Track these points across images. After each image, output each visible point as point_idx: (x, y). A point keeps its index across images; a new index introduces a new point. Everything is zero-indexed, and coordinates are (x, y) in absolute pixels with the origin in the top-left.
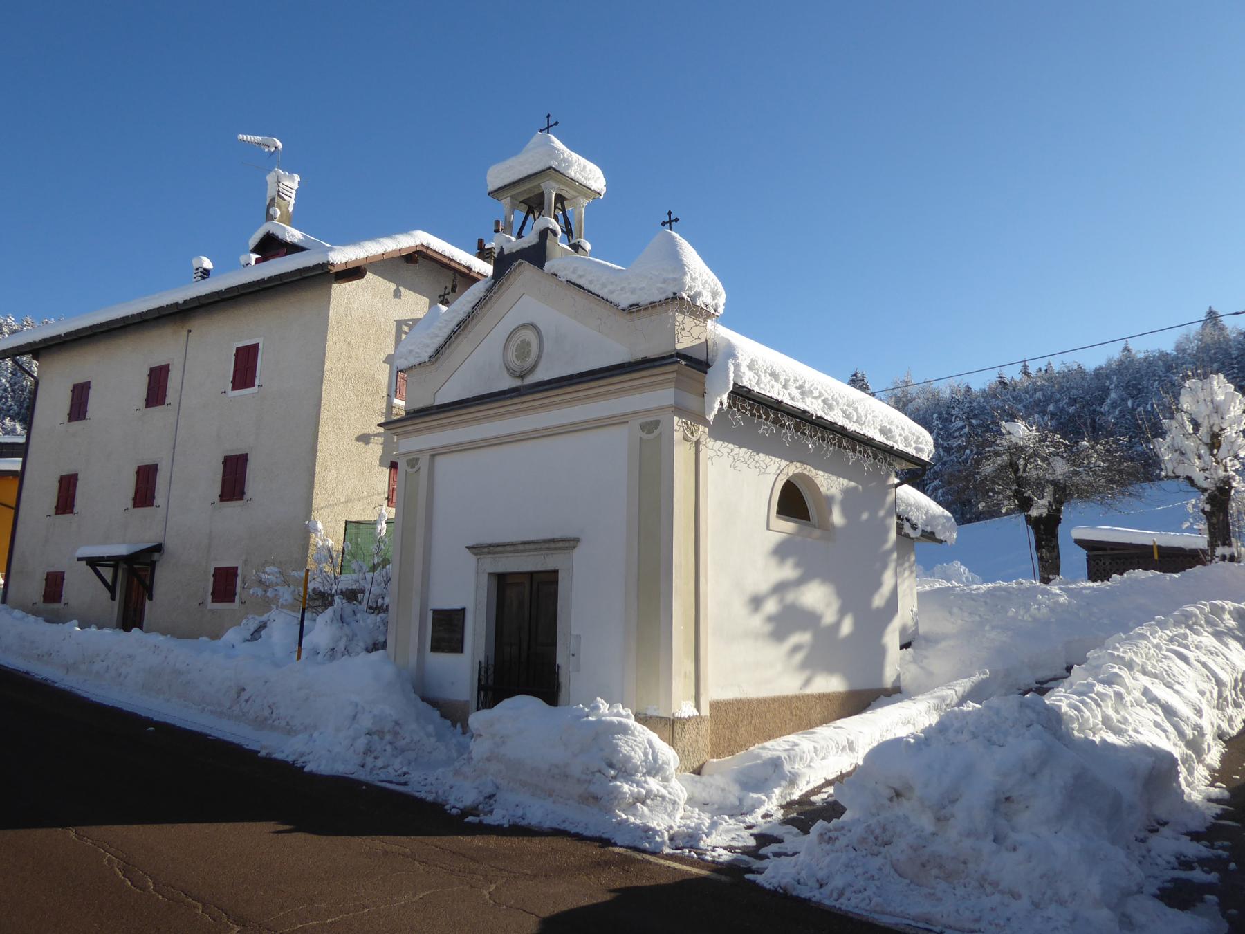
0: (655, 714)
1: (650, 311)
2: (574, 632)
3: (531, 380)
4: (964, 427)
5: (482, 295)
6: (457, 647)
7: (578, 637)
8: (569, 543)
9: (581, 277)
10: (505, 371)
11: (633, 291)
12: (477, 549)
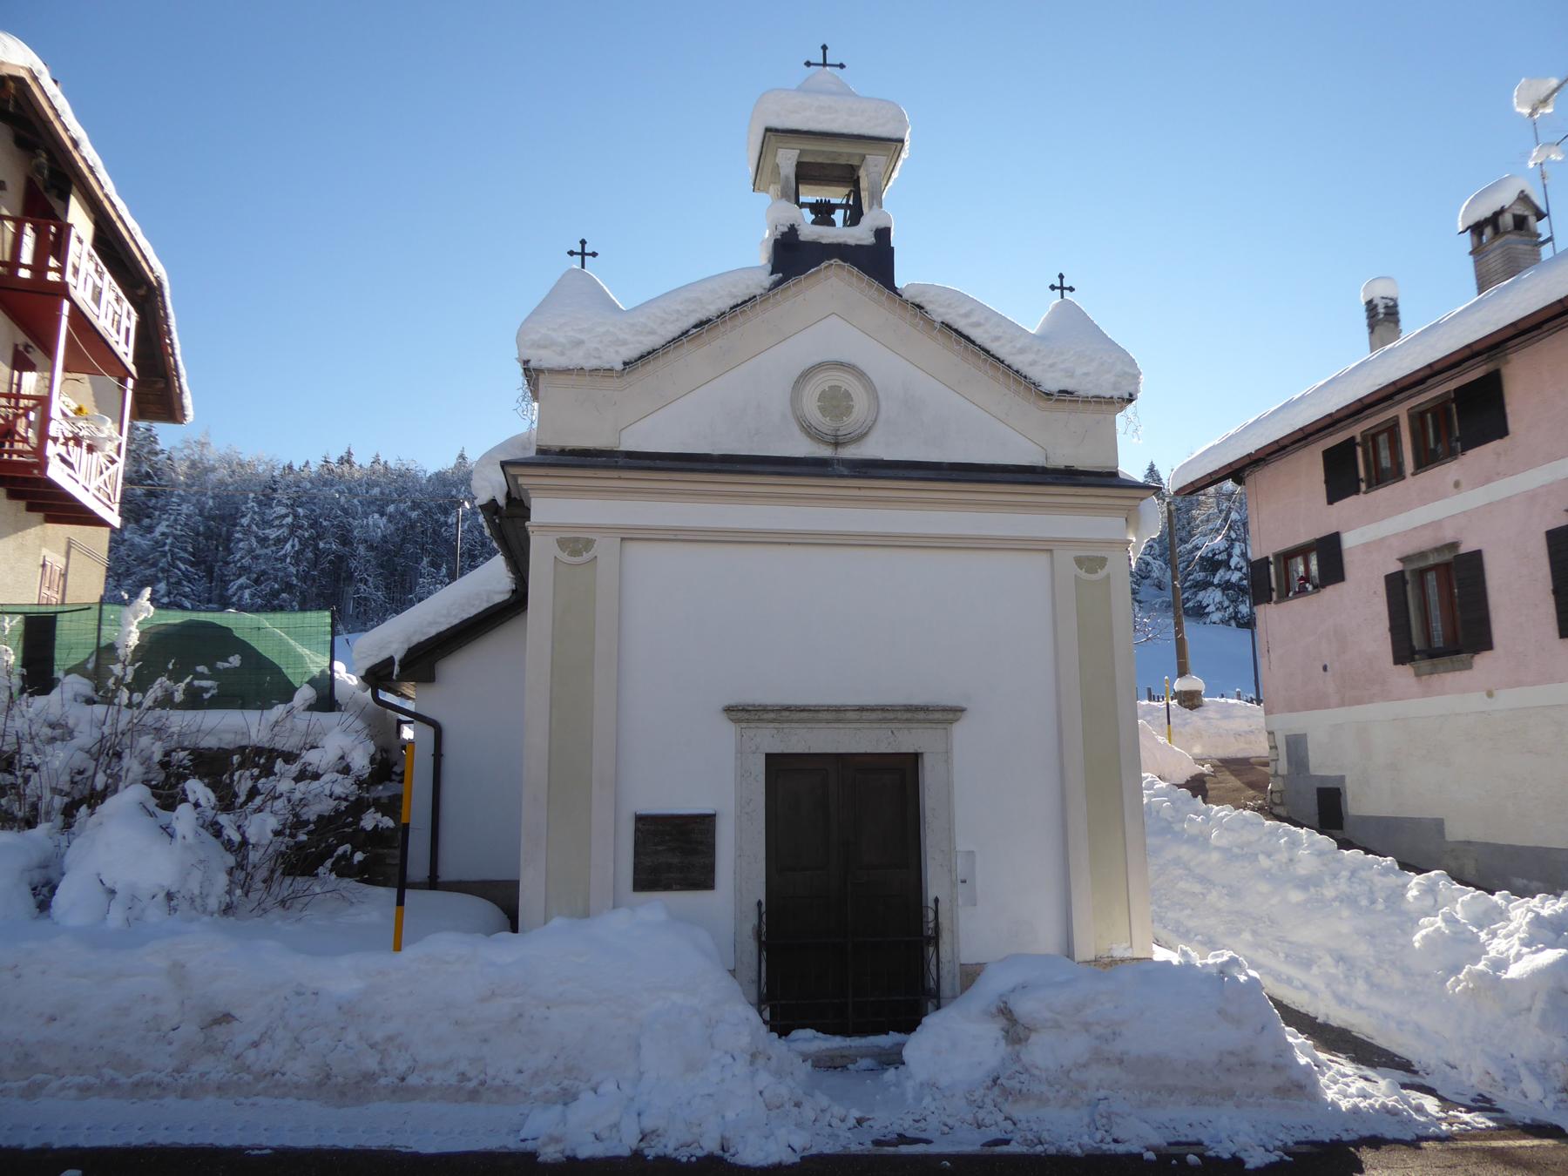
0: (1128, 954)
1: (1092, 407)
2: (962, 845)
3: (849, 453)
4: (286, 516)
5: (758, 291)
6: (702, 878)
7: (971, 853)
8: (951, 714)
9: (978, 325)
10: (796, 429)
11: (1070, 374)
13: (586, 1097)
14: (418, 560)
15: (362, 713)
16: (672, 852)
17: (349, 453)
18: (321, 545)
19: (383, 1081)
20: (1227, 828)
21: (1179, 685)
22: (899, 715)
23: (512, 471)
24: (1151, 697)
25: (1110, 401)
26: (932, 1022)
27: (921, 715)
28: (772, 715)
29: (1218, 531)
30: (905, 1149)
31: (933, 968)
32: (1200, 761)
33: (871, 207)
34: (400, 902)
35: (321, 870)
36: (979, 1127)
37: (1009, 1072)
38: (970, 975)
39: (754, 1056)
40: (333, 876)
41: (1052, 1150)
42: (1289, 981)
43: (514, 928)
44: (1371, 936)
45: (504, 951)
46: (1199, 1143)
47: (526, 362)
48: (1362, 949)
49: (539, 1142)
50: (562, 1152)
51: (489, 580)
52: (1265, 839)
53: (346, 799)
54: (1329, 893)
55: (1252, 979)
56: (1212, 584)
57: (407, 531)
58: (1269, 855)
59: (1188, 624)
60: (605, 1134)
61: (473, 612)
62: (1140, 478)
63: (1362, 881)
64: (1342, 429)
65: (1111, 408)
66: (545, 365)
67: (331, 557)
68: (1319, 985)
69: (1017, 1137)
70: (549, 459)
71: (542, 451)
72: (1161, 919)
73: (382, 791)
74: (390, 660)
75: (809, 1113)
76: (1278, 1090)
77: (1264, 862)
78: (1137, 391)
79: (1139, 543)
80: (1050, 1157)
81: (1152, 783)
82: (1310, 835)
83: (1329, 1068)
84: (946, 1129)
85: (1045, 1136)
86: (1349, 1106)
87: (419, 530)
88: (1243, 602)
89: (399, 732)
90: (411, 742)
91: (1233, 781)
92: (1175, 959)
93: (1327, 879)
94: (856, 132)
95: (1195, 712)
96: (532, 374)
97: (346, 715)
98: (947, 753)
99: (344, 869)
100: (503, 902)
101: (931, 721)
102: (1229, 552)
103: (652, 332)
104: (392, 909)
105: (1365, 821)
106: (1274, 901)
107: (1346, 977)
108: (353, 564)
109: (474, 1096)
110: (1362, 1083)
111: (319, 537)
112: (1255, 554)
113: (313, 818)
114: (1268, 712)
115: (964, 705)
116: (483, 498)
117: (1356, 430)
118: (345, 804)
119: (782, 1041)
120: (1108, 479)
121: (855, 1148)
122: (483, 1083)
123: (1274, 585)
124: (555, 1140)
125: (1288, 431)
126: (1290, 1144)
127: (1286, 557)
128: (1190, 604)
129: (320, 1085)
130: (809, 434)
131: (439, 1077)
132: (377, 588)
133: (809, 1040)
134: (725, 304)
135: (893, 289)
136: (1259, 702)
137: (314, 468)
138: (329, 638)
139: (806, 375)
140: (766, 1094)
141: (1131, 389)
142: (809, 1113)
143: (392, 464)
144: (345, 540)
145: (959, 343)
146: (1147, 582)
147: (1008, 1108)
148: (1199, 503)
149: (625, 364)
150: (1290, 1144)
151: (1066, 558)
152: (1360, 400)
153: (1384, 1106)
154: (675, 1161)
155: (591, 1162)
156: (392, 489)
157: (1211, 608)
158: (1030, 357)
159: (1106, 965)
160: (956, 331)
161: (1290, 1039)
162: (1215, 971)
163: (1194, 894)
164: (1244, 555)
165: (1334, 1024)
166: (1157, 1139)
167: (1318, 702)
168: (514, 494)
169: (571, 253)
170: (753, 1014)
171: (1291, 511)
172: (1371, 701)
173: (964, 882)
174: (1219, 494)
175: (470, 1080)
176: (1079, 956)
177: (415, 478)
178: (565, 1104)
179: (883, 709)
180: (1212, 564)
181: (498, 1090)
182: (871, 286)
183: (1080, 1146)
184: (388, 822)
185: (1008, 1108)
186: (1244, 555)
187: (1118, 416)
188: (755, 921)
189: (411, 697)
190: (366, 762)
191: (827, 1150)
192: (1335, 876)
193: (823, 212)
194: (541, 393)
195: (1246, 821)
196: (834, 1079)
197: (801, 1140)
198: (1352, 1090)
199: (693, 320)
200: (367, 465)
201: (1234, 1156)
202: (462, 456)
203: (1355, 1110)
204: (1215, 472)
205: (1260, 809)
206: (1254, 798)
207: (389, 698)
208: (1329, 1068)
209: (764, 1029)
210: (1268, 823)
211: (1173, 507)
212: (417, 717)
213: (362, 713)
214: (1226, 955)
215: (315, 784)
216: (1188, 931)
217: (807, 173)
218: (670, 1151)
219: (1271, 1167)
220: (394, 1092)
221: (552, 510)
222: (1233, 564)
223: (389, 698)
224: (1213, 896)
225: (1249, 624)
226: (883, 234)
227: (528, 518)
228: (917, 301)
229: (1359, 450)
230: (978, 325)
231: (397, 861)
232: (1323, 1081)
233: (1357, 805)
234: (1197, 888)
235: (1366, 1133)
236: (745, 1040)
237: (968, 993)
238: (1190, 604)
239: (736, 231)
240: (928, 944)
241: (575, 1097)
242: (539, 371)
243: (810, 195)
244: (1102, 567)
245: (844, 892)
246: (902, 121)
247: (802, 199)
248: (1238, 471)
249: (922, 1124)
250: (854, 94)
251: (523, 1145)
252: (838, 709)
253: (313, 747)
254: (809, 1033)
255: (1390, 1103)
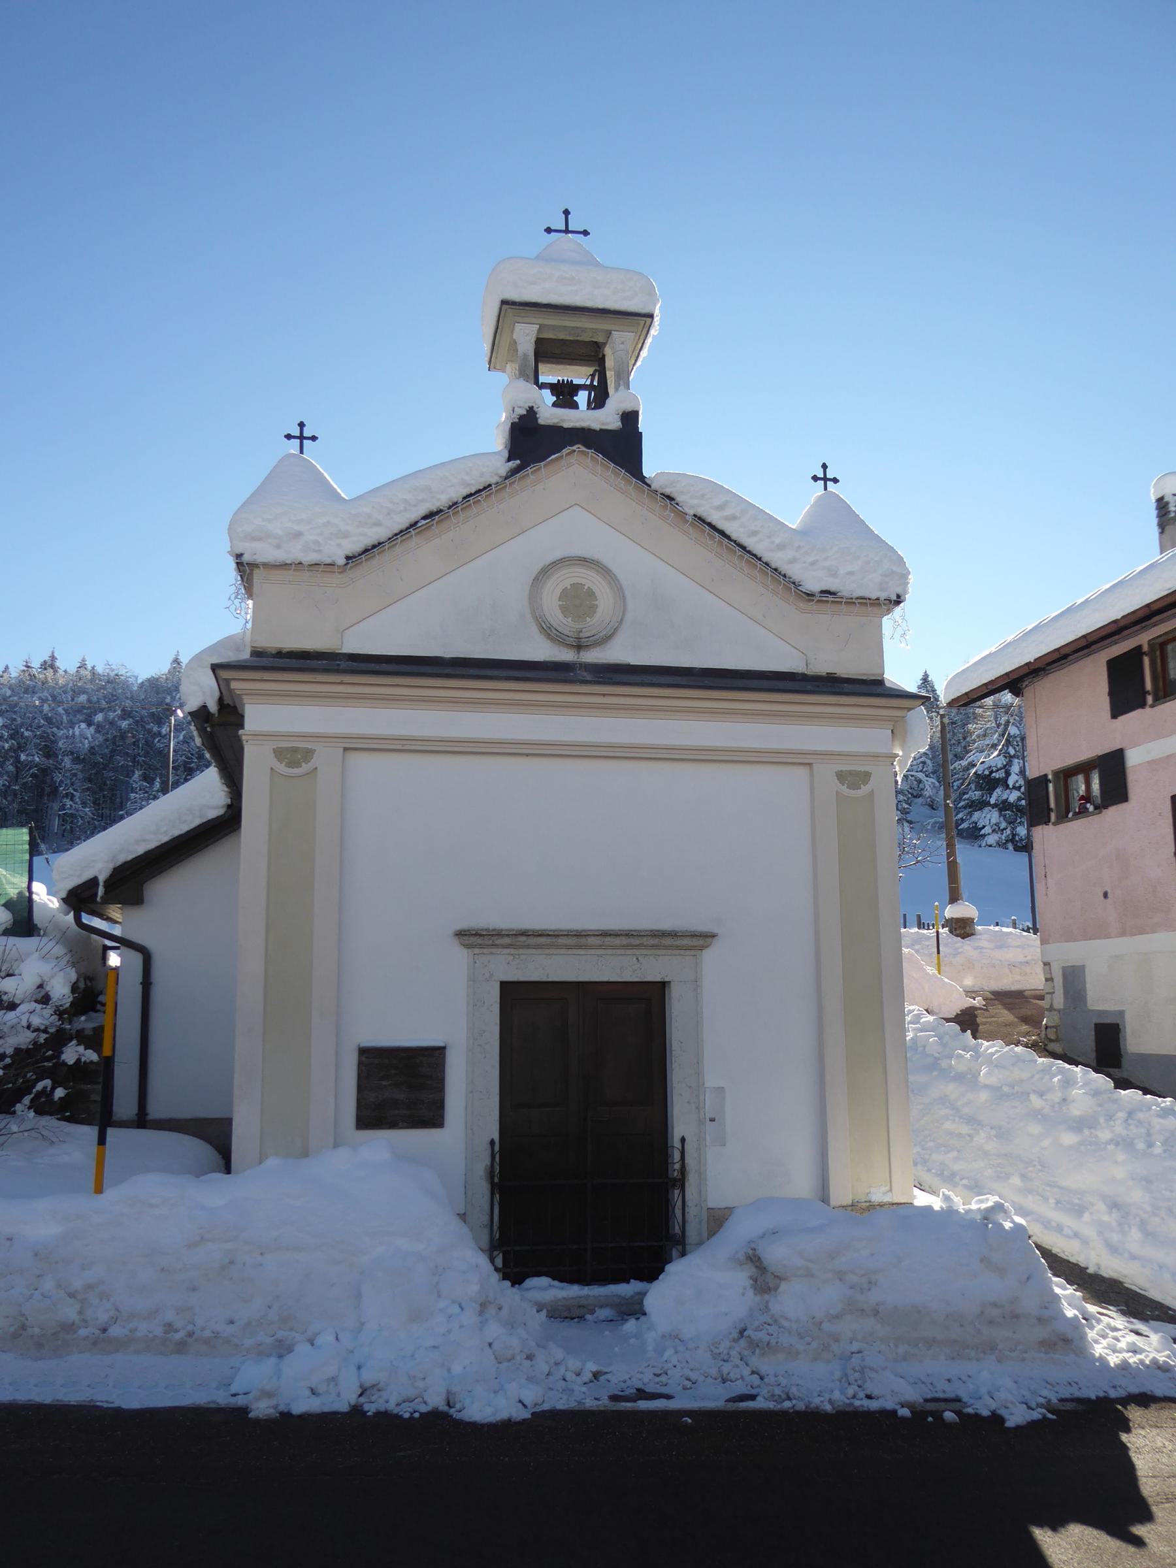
0: (887, 1199)
1: (856, 609)
2: (711, 1080)
3: (592, 656)
5: (493, 480)
9: (733, 518)
10: (535, 629)
11: (834, 573)
12: (470, 937)
13: (302, 1349)
14: (129, 774)
15: (64, 937)
16: (399, 1087)
17: (53, 658)
18: (23, 757)
19: (83, 1332)
20: (996, 1065)
21: (951, 912)
22: (645, 941)
23: (224, 674)
24: (921, 925)
25: (876, 602)
26: (676, 1270)
27: (668, 941)
28: (507, 940)
29: (994, 746)
30: (643, 1405)
31: (678, 1212)
32: (971, 993)
33: (617, 389)
34: (102, 1141)
35: (19, 1107)
36: (724, 1381)
37: (756, 1323)
38: (718, 1220)
39: (483, 1306)
40: (32, 1114)
41: (801, 1406)
42: (1059, 1229)
43: (228, 1170)
44: (1147, 1181)
45: (216, 1193)
46: (958, 1400)
47: (239, 556)
48: (1137, 1196)
49: (250, 1396)
50: (275, 1407)
51: (203, 794)
52: (1037, 1076)
53: (45, 1031)
54: (1104, 1135)
55: (1018, 1226)
56: (988, 804)
57: (116, 743)
58: (1041, 1095)
59: (961, 847)
60: (322, 1388)
61: (185, 828)
62: (912, 687)
63: (1140, 1123)
64: (1128, 637)
65: (876, 610)
66: (260, 559)
67: (34, 770)
68: (1090, 1232)
69: (764, 1392)
70: (265, 662)
71: (257, 653)
72: (925, 1162)
73: (84, 1022)
74: (94, 882)
75: (541, 1365)
76: (1042, 1343)
77: (1036, 1102)
78: (906, 592)
79: (906, 756)
80: (798, 1413)
81: (919, 1016)
82: (1086, 1073)
83: (1099, 1321)
84: (688, 1384)
85: (794, 1391)
86: (1117, 1361)
87: (130, 741)
88: (1021, 823)
89: (104, 958)
90: (116, 969)
91: (1006, 1016)
92: (937, 1203)
93: (1102, 1120)
94: (601, 306)
95: (967, 941)
96: (246, 569)
97: (45, 940)
98: (696, 982)
99: (43, 1106)
100: (215, 1138)
101: (678, 948)
102: (1007, 769)
103: (378, 524)
104: (94, 1149)
105: (1144, 1058)
106: (1045, 1143)
107: (1120, 1224)
108: (58, 777)
109: (181, 1348)
110: (1132, 1338)
111: (21, 748)
112: (1032, 773)
113: (10, 1051)
114: (1043, 942)
115: (715, 931)
116: (193, 704)
117: (1143, 639)
118: (45, 1036)
119: (515, 1290)
120: (872, 688)
121: (590, 1404)
122: (191, 1334)
123: (1052, 805)
124: (269, 1394)
125: (1070, 638)
126: (1054, 1401)
127: (1066, 775)
128: (965, 825)
129: (15, 1336)
130: (548, 636)
131: (143, 1328)
132: (84, 804)
133: (545, 1289)
134: (457, 493)
135: (642, 478)
136: (1036, 931)
137: (14, 673)
138: (27, 857)
139: (545, 572)
140: (495, 1346)
141: (899, 590)
142: (541, 1365)
143: (100, 669)
144: (49, 751)
145: (712, 538)
146: (920, 800)
147: (755, 1361)
148: (976, 717)
149: (348, 558)
150: (1054, 1401)
151: (826, 772)
152: (1148, 605)
153: (1154, 1361)
154: (397, 1417)
155: (306, 1418)
156: (101, 696)
157: (987, 830)
158: (790, 554)
159: (863, 1210)
160: (709, 524)
161: (1057, 1290)
162: (978, 1217)
163: (960, 1135)
164: (1022, 772)
165: (1104, 1274)
166: (913, 1395)
167: (1096, 931)
168: (227, 701)
169: (289, 437)
170: (483, 1261)
171: (1071, 726)
172: (1153, 931)
173: (712, 1120)
174: (996, 706)
175: (176, 1331)
176: (833, 1202)
177: (126, 685)
178: (280, 1356)
179: (628, 934)
180: (988, 782)
181: (207, 1341)
182: (617, 475)
183: (830, 1401)
184: (91, 1056)
185: (755, 1361)
186: (1022, 772)
187: (885, 619)
188: (488, 1162)
189: (117, 921)
190: (66, 990)
191: (561, 1405)
192: (1110, 1117)
193: (565, 394)
194: (256, 589)
195: (1018, 1059)
196: (570, 1330)
197: (531, 1395)
198: (1122, 1345)
199: (422, 510)
200: (72, 669)
201: (994, 1413)
202: (176, 661)
203: (1124, 1366)
204: (991, 682)
205: (1033, 1046)
206: (1027, 1034)
207: (97, 923)
208: (1099, 1321)
209: (495, 1277)
210: (1041, 1060)
211: (946, 720)
212: (124, 943)
213: (64, 937)
214: (991, 1200)
215: (11, 1016)
216: (954, 1175)
217: (546, 351)
218: (391, 1407)
219: (1033, 1424)
220: (95, 1343)
221: (266, 717)
222: (1011, 782)
223: (97, 923)
224: (980, 1138)
225: (1025, 847)
226: (630, 418)
227: (242, 726)
228: (668, 491)
229: (1146, 660)
230: (733, 518)
231: (98, 1098)
232: (1091, 1335)
233: (1139, 1041)
234: (964, 1129)
235: (1134, 1390)
236: (473, 1289)
237: (714, 1239)
238: (965, 825)
239: (470, 413)
240: (674, 1186)
241: (290, 1350)
242: (253, 565)
243: (551, 374)
244: (866, 782)
245: (583, 1126)
246: (652, 293)
247: (543, 379)
248: (1015, 682)
249: (663, 1379)
250: (598, 264)
251: (233, 1400)
252: (579, 934)
253: (9, 975)
254: (544, 1281)
255: (1161, 1358)
